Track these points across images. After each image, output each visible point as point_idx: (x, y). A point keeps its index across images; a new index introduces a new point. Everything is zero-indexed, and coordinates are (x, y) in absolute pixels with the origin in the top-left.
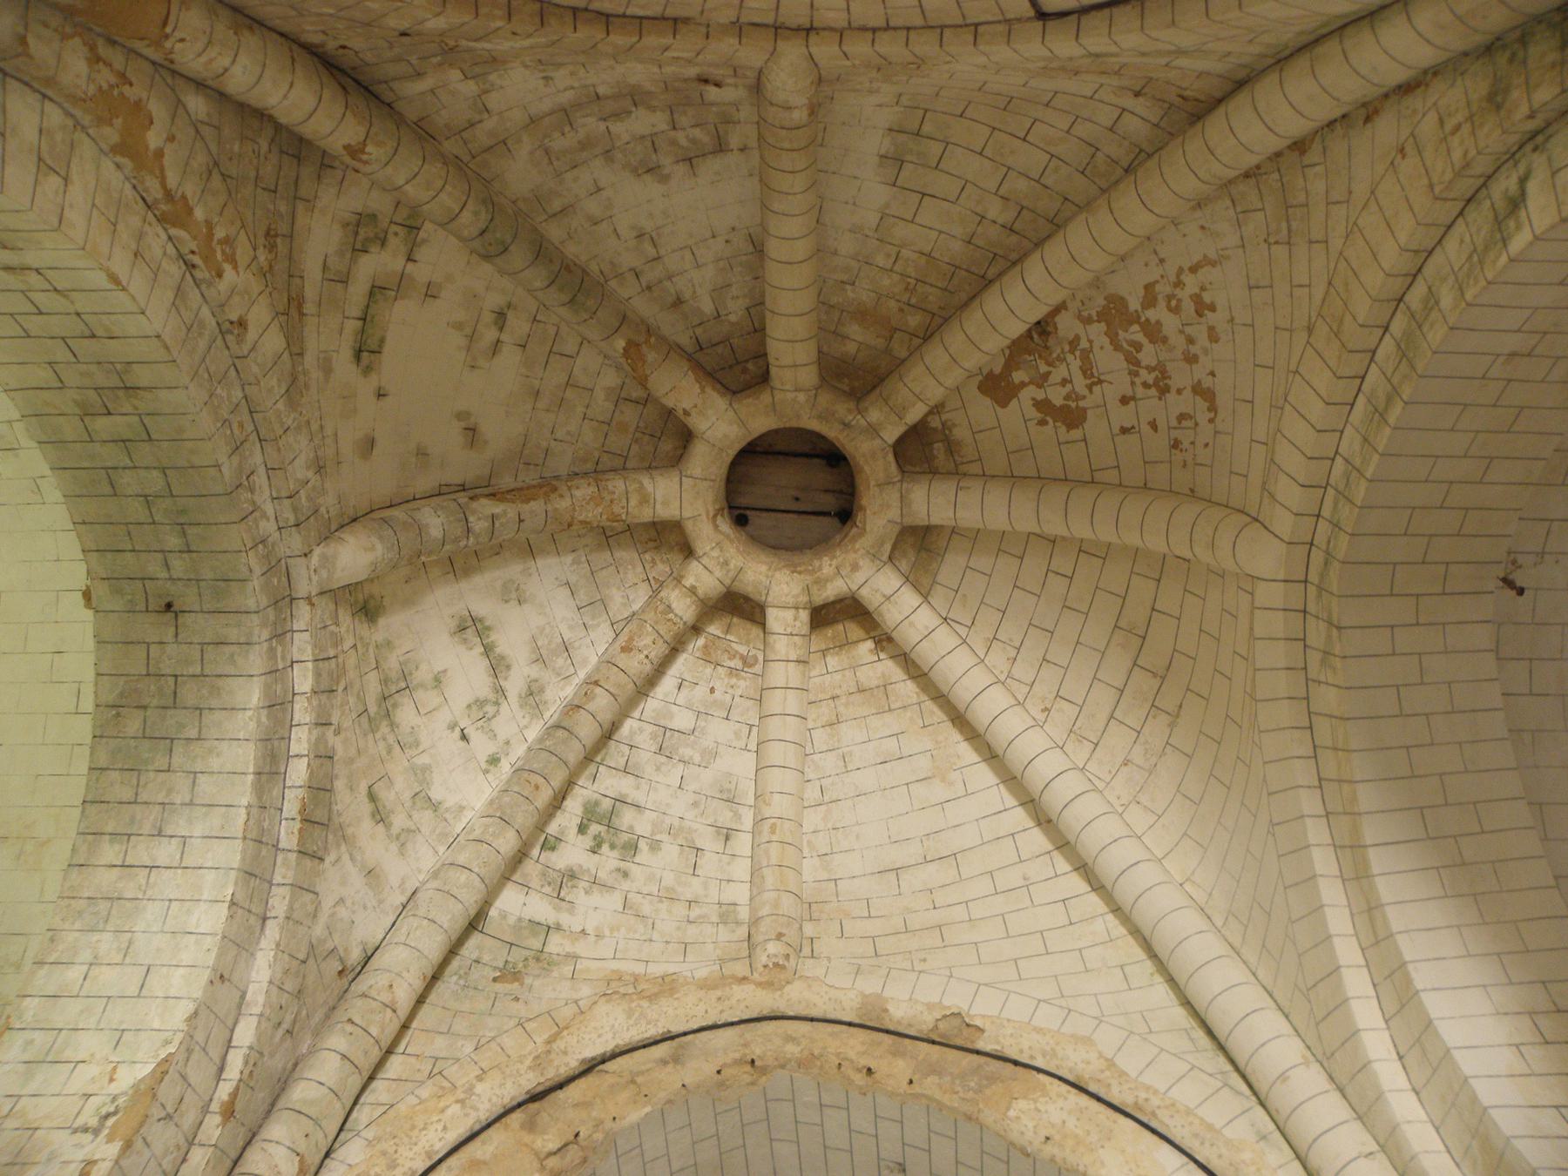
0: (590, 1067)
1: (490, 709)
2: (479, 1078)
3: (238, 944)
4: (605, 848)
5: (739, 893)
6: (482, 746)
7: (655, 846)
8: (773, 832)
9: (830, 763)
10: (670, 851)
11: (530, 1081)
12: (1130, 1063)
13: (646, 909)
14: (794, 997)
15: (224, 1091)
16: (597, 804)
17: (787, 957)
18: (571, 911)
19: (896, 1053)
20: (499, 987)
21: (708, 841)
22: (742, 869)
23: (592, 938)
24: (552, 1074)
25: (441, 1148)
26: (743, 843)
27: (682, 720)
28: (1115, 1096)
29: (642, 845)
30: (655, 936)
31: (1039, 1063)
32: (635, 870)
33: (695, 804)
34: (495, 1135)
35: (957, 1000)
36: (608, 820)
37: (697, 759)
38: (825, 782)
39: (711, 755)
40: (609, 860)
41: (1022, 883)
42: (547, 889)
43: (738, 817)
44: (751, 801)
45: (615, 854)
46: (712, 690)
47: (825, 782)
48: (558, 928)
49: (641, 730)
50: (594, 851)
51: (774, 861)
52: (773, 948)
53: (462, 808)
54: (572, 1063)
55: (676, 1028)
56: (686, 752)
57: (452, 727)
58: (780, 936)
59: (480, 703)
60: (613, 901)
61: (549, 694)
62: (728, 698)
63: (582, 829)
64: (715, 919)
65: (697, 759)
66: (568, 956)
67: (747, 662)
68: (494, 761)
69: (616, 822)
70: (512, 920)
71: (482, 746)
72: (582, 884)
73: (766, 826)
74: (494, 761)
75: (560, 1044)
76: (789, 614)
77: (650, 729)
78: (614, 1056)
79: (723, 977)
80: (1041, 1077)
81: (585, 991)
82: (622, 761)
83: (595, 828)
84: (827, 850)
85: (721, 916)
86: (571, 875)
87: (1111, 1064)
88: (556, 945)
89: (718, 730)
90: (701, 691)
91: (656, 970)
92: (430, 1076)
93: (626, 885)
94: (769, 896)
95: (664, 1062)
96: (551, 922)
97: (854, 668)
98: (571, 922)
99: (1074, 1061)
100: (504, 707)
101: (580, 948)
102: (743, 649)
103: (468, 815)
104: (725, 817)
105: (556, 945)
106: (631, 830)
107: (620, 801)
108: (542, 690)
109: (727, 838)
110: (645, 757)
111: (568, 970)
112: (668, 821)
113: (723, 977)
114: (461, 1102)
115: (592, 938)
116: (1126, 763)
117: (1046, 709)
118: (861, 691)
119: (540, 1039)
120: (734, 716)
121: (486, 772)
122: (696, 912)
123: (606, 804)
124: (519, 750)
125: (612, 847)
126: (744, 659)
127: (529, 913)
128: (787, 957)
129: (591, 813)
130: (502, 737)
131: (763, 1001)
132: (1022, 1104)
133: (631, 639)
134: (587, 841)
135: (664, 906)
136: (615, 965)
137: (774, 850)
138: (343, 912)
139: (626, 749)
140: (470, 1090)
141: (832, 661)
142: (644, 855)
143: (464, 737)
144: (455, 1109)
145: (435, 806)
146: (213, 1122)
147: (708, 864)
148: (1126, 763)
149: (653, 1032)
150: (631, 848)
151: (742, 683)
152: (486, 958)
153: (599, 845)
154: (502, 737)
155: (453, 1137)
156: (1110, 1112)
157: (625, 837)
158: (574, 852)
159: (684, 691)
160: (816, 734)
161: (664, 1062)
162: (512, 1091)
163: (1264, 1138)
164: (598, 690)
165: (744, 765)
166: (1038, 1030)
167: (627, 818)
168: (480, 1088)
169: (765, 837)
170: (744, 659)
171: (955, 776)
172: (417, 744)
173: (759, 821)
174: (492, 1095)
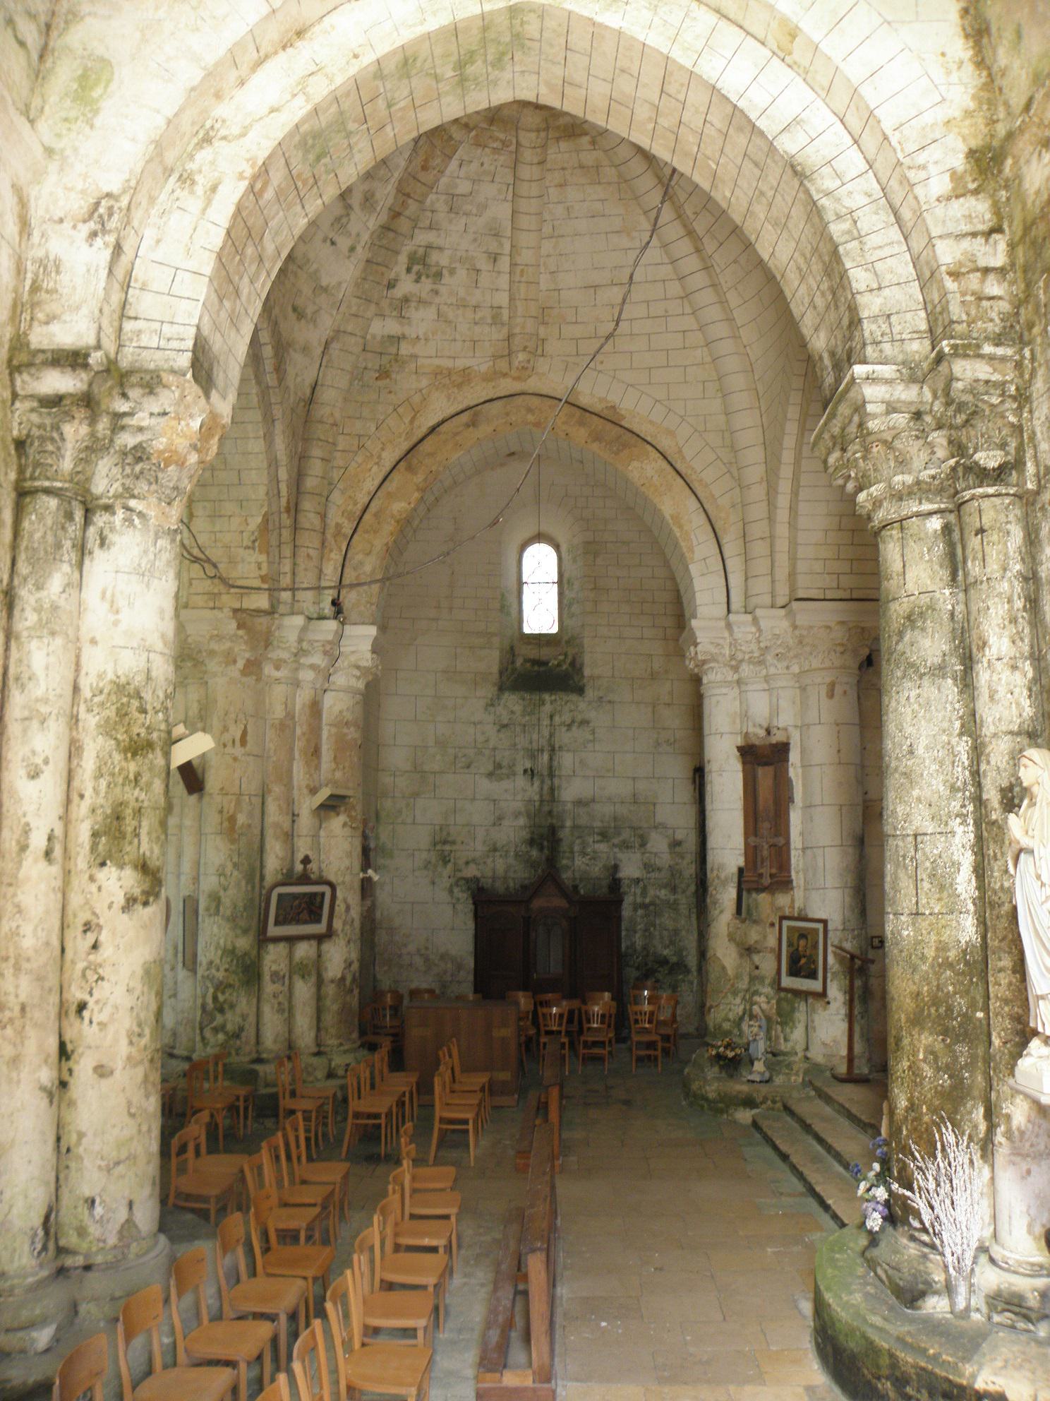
0: (433, 430)
1: (344, 220)
2: (383, 449)
3: (269, 438)
4: (423, 278)
5: (502, 299)
6: (344, 243)
7: (452, 272)
8: (522, 276)
9: (559, 210)
10: (462, 273)
11: (406, 446)
12: (688, 452)
13: (451, 315)
14: (532, 384)
15: (284, 501)
16: (415, 252)
17: (529, 361)
18: (409, 324)
19: (581, 423)
20: (379, 383)
21: (483, 264)
22: (504, 281)
23: (423, 342)
24: (415, 439)
25: (373, 489)
26: (504, 263)
27: (464, 187)
28: (678, 466)
29: (445, 272)
30: (458, 337)
31: (649, 439)
32: (443, 290)
33: (475, 240)
34: (396, 476)
35: (613, 398)
36: (423, 261)
37: (474, 211)
38: (556, 223)
39: (483, 207)
40: (427, 284)
41: (663, 313)
42: (395, 313)
43: (501, 245)
44: (509, 234)
45: (430, 280)
46: (482, 164)
47: (556, 223)
48: (404, 337)
49: (438, 200)
50: (417, 281)
51: (522, 296)
52: (521, 357)
53: (340, 284)
54: (424, 430)
55: (472, 404)
56: (468, 207)
57: (324, 240)
58: (525, 348)
59: (338, 219)
60: (430, 313)
61: (378, 196)
62: (493, 168)
63: (409, 270)
64: (489, 321)
65: (474, 211)
66: (411, 356)
67: (505, 144)
68: (352, 249)
69: (428, 261)
70: (379, 338)
71: (344, 243)
72: (413, 304)
73: (518, 269)
74: (352, 249)
75: (416, 423)
76: (533, 135)
77: (444, 197)
78: (443, 422)
79: (495, 373)
80: (648, 447)
81: (424, 382)
82: (428, 223)
83: (416, 268)
84: (555, 269)
85: (493, 318)
86: (406, 300)
87: (680, 451)
88: (405, 349)
89: (488, 190)
90: (474, 166)
91: (460, 363)
92: (359, 448)
93: (437, 300)
94: (519, 320)
95: (468, 426)
96: (399, 333)
97: (578, 151)
98: (411, 332)
99: (665, 443)
100: (353, 217)
101: (419, 349)
102: (502, 136)
103: (344, 285)
104: (493, 247)
105: (405, 349)
106: (437, 264)
107: (429, 247)
108: (373, 195)
109: (495, 260)
110: (441, 216)
111: (413, 366)
112: (459, 254)
113: (495, 373)
114: (377, 464)
115: (423, 342)
116: (735, 262)
117: (695, 213)
118: (581, 167)
119: (407, 420)
120: (497, 179)
121: (349, 257)
122: (479, 315)
123: (421, 251)
124: (365, 237)
125: (428, 276)
126: (503, 142)
127: (387, 331)
128: (529, 361)
129: (413, 259)
130: (354, 233)
131: (517, 387)
132: (635, 464)
133: (426, 160)
134: (413, 276)
135: (460, 312)
136: (437, 362)
137: (523, 288)
138: (299, 379)
139: (429, 214)
140: (379, 457)
141: (564, 145)
142: (446, 279)
143: (333, 243)
144: (375, 469)
145: (325, 290)
146: (284, 516)
147: (485, 280)
148: (735, 262)
149: (461, 407)
150: (439, 275)
151: (502, 158)
152: (370, 365)
153: (419, 277)
154: (354, 233)
155: (377, 483)
156: (674, 473)
157: (434, 270)
158: (406, 286)
159: (464, 169)
160: (551, 190)
161: (468, 426)
162: (398, 454)
163: (733, 506)
164: (410, 201)
165: (502, 211)
166: (651, 422)
167: (434, 257)
168: (384, 454)
169: (517, 278)
170: (503, 142)
171: (635, 234)
172: (308, 260)
173: (513, 265)
174: (389, 458)
